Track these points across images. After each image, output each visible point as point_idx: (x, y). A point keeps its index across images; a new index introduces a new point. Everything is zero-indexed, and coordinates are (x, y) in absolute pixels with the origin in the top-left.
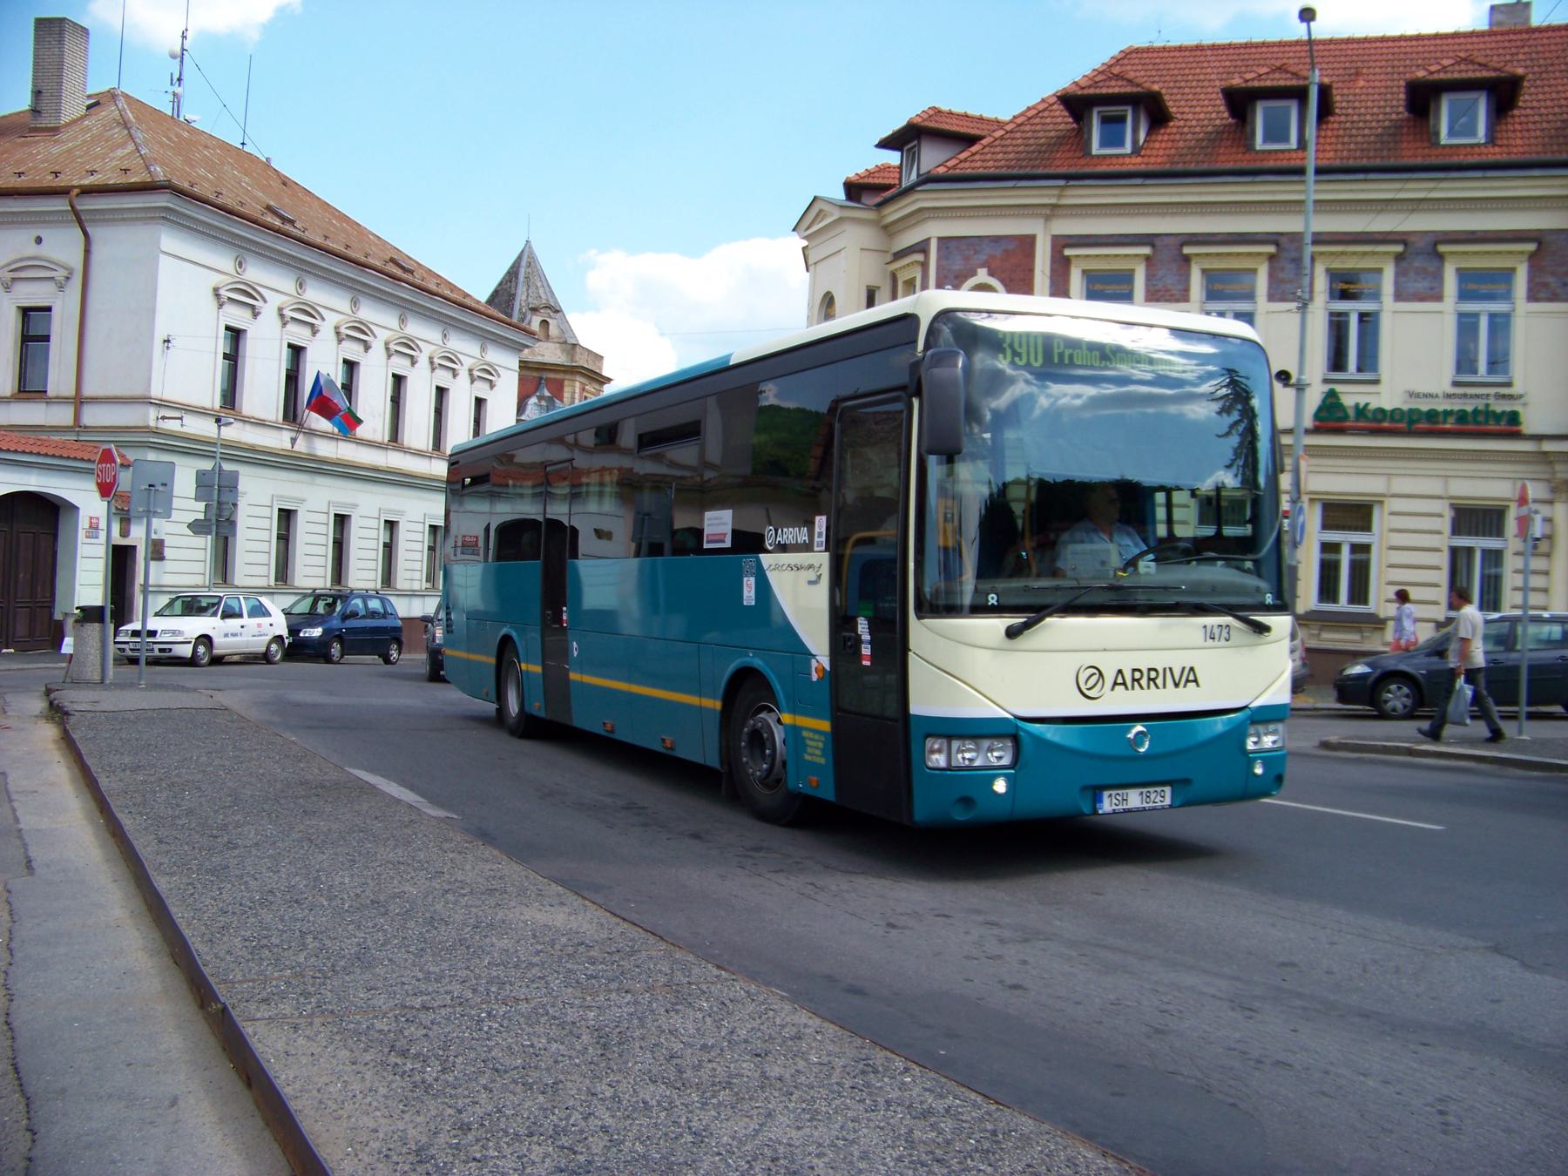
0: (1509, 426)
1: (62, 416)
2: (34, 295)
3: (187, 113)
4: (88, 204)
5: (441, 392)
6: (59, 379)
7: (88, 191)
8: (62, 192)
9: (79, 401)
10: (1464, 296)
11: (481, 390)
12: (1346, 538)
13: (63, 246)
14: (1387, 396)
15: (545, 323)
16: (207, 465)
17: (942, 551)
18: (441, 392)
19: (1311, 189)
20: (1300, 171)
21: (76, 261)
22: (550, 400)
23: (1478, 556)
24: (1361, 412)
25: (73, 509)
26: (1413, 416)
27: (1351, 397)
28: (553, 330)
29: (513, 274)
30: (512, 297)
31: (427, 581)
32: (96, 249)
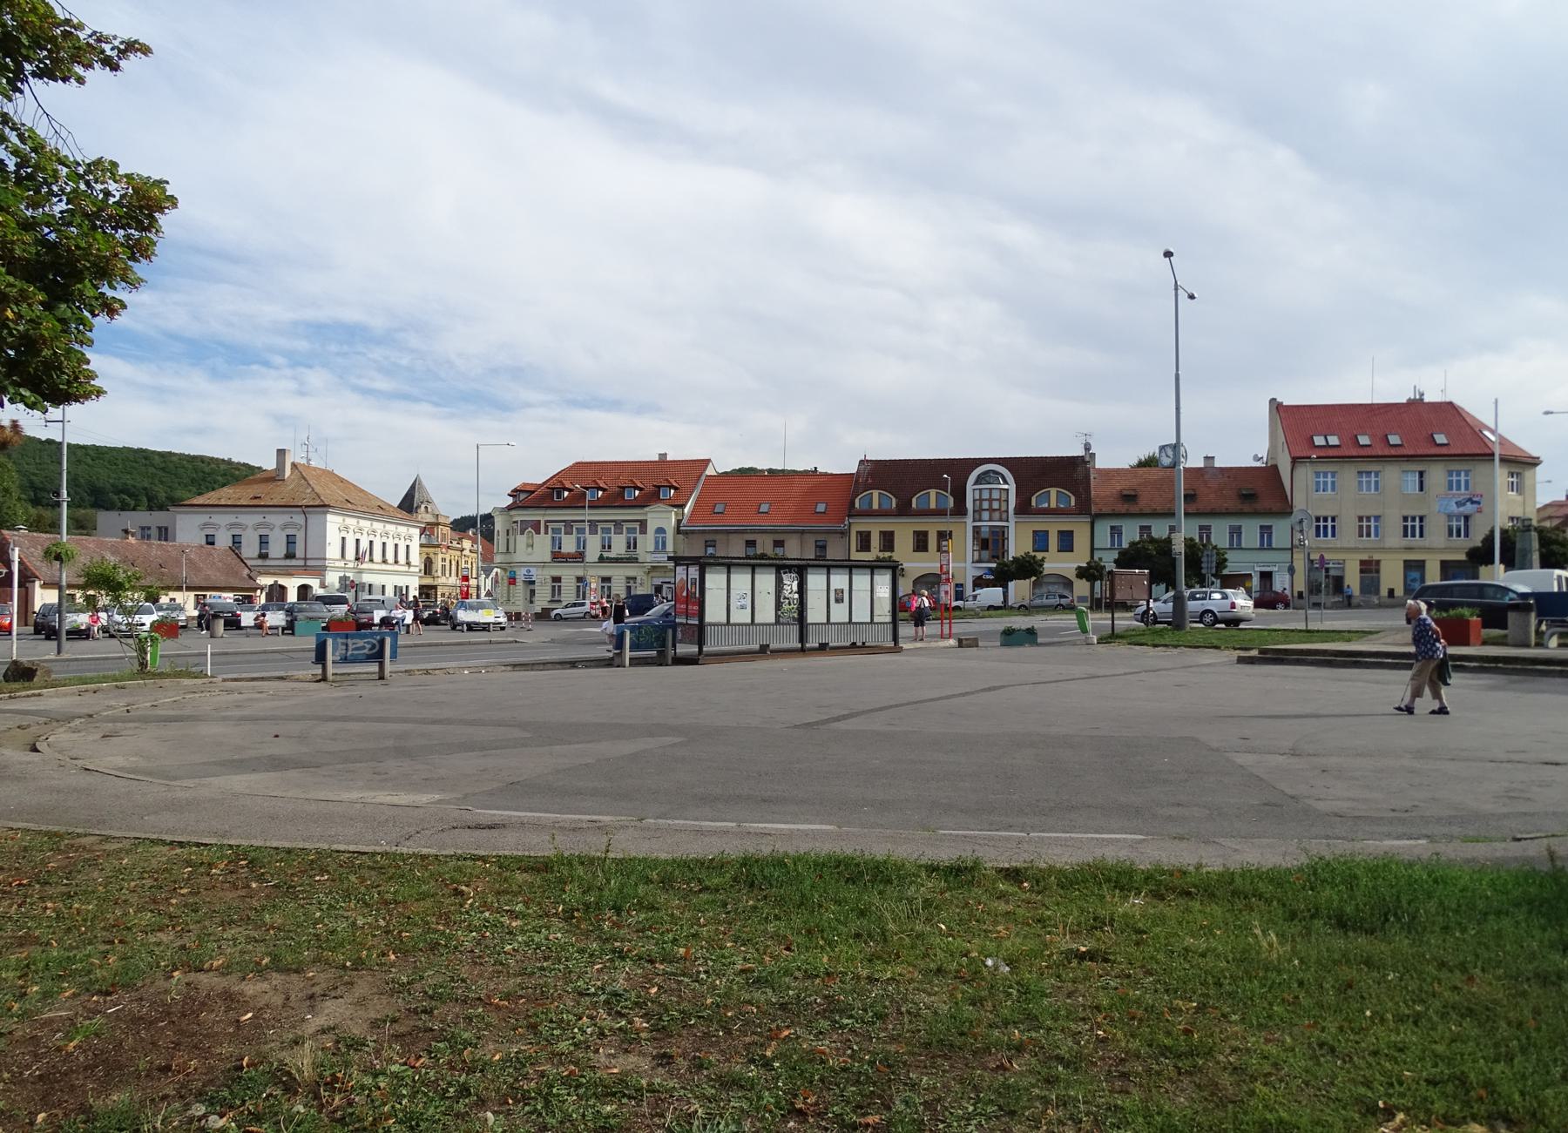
0: (635, 560)
1: (301, 563)
2: (290, 532)
3: (313, 463)
4: (306, 510)
5: (396, 545)
6: (299, 553)
7: (307, 506)
8: (301, 506)
9: (305, 559)
10: (628, 533)
11: (408, 542)
12: (606, 585)
13: (299, 519)
14: (612, 555)
15: (426, 508)
16: (342, 574)
17: (1252, 492)
18: (396, 545)
19: (587, 511)
20: (584, 507)
21: (303, 524)
22: (429, 536)
23: (963, 565)
24: (607, 558)
25: (311, 587)
26: (617, 559)
27: (605, 555)
28: (429, 510)
29: (413, 487)
30: (413, 497)
31: (1275, 608)
32: (309, 521)
